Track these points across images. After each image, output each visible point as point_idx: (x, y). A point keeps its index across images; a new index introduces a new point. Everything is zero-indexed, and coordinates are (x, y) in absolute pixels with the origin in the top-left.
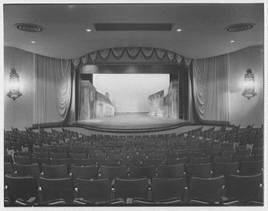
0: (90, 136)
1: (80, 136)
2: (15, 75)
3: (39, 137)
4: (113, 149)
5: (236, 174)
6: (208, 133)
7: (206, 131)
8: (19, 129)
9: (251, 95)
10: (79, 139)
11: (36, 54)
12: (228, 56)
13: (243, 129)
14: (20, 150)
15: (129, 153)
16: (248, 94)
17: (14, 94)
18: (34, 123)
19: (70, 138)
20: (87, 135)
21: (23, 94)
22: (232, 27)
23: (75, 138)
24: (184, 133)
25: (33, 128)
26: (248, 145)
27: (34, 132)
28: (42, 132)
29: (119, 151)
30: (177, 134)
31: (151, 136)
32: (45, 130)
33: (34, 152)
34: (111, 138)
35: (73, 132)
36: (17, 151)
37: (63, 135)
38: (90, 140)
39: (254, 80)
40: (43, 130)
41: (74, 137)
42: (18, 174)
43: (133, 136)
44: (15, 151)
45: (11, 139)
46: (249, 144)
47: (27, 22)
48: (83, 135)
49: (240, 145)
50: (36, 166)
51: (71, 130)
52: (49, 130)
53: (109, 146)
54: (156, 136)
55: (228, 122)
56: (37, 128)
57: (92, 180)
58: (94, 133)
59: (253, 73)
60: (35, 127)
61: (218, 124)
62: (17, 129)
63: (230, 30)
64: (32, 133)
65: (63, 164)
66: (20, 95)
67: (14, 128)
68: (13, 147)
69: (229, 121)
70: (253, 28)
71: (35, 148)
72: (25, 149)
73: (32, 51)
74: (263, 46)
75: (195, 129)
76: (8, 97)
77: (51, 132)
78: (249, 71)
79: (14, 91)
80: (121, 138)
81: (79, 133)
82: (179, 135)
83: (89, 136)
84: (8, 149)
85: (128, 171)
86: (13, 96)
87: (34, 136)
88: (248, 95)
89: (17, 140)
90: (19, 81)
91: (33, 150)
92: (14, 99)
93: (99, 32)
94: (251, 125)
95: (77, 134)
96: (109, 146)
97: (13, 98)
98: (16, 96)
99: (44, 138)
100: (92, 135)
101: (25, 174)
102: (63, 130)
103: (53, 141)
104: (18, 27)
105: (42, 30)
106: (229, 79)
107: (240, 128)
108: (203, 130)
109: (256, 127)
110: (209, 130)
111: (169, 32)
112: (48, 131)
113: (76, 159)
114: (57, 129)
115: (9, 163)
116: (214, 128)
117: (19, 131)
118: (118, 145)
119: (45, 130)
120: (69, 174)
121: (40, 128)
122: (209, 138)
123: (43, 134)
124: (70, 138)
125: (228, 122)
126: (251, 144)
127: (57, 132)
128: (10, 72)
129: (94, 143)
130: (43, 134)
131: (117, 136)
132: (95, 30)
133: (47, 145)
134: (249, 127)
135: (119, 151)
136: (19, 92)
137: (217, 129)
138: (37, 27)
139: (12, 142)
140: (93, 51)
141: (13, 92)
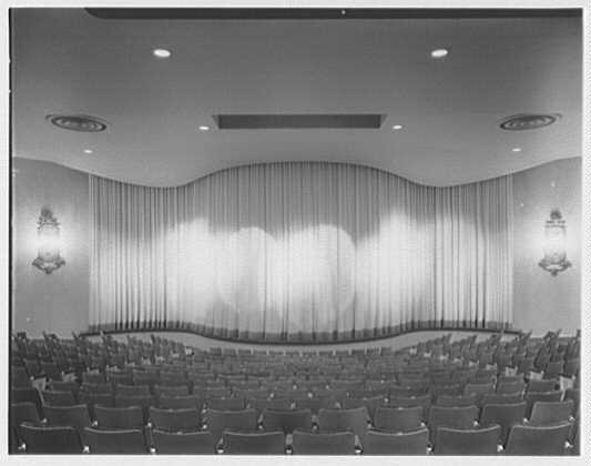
0: (208, 350)
1: (188, 352)
2: (49, 221)
3: (99, 352)
4: (277, 380)
5: (472, 427)
6: (458, 347)
7: (455, 344)
8: (59, 337)
9: (557, 267)
10: (183, 358)
11: (95, 176)
12: (510, 180)
13: (537, 340)
14: (58, 378)
15: (312, 385)
16: (553, 263)
17: (48, 262)
18: (92, 323)
19: (166, 354)
20: (203, 350)
21: (67, 261)
22: (512, 121)
23: (176, 355)
24: (409, 348)
25: (88, 334)
26: (562, 378)
27: (90, 343)
28: (108, 342)
29: (256, 382)
30: (394, 350)
31: (337, 353)
32: (116, 338)
33: (84, 383)
34: (253, 357)
35: (173, 344)
36: (51, 380)
37: (151, 349)
38: (206, 360)
39: (565, 232)
40: (109, 337)
41: (175, 352)
42: (48, 425)
43: (298, 353)
44: (47, 380)
45: (23, 355)
46: (564, 376)
47: (73, 114)
48: (193, 349)
49: (544, 378)
50: (84, 409)
51: (169, 339)
52: (121, 339)
53: (241, 373)
54: (347, 352)
55: (507, 324)
56: (98, 334)
57: (179, 433)
58: (216, 344)
59: (564, 218)
60: (94, 332)
61: (216, 333)
62: (54, 336)
63: (507, 126)
64: (83, 343)
65: (134, 405)
66: (60, 263)
67: (47, 333)
68: (43, 372)
69: (510, 322)
70: (556, 122)
71: (87, 377)
72: (69, 378)
73: (86, 170)
74: (579, 159)
75: (466, 338)
76: (36, 268)
77: (126, 342)
78: (556, 215)
79: (48, 254)
80: (273, 357)
81: (185, 344)
82: (397, 353)
83: (205, 352)
84: (32, 378)
85: (260, 421)
86: (46, 265)
87: (88, 350)
88: (552, 267)
89: (53, 358)
90: (58, 233)
91: (84, 379)
92: (48, 271)
93: (224, 131)
94: (554, 331)
95: (181, 347)
96: (241, 373)
97: (46, 269)
98: (52, 265)
99: (109, 355)
100: (212, 349)
101: (63, 423)
102: (153, 337)
103: (129, 362)
104: (54, 122)
105: (104, 127)
106: (511, 228)
107: (532, 336)
108: (478, 341)
109: (566, 336)
110: (463, 342)
111: (376, 130)
112: (119, 341)
113: (163, 396)
114: (139, 336)
115: (30, 404)
116: (475, 337)
117: (27, 341)
118: (262, 370)
119: (116, 338)
120: (146, 424)
121: (104, 333)
122: (459, 357)
123: (109, 348)
124: (166, 354)
125: (507, 324)
126: (570, 377)
127: (166, 341)
128: (40, 214)
129: (212, 367)
130: (109, 348)
131: (265, 353)
132: (217, 128)
133: (116, 369)
134: (550, 334)
135: (256, 382)
136: (58, 258)
137: (482, 338)
138: (94, 122)
139: (42, 363)
140: (190, 180)
141: (46, 258)
